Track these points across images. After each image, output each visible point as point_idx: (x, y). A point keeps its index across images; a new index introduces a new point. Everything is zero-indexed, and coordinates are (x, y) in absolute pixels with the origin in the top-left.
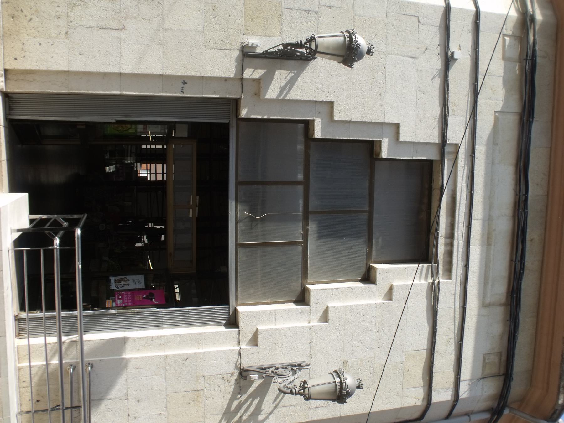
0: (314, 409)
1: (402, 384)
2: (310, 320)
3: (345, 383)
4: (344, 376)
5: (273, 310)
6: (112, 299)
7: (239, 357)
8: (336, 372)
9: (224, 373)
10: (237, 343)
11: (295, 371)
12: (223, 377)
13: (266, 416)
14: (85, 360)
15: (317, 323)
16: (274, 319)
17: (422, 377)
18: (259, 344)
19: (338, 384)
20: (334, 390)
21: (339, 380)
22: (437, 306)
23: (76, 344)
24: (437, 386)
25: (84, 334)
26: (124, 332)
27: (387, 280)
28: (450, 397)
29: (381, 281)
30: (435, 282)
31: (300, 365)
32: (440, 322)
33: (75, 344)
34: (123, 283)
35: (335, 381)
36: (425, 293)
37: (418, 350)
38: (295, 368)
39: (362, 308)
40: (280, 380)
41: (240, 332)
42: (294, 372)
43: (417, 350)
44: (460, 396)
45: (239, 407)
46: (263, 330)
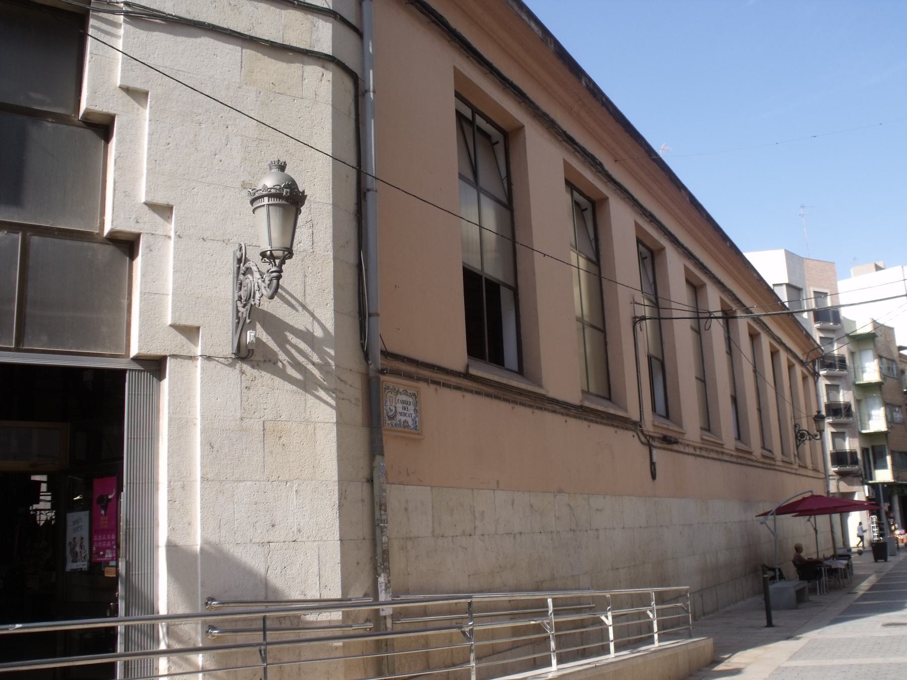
0: (314, 246)
1: (294, 98)
2: (166, 236)
3: (271, 188)
4: (260, 190)
5: (141, 297)
6: (105, 567)
7: (215, 360)
8: (252, 202)
9: (239, 386)
10: (190, 361)
11: (247, 269)
12: (246, 388)
13: (316, 324)
14: (200, 611)
15: (171, 224)
16: (156, 296)
17: (287, 63)
18: (196, 324)
19: (272, 201)
20: (281, 209)
21: (266, 199)
22: (169, 15)
23: (172, 625)
24: (306, 42)
25: (158, 612)
26: (158, 546)
27: (111, 94)
28: (327, 23)
29: (111, 105)
30: (124, 9)
31: (239, 261)
32: (198, 16)
33: (172, 627)
34: (78, 549)
35: (266, 206)
36: (142, 31)
37: (242, 62)
38: (243, 268)
39: (154, 145)
40: (258, 295)
41: (173, 355)
42: (248, 271)
43: (240, 64)
44: (329, 6)
45: (297, 365)
46: (172, 316)
